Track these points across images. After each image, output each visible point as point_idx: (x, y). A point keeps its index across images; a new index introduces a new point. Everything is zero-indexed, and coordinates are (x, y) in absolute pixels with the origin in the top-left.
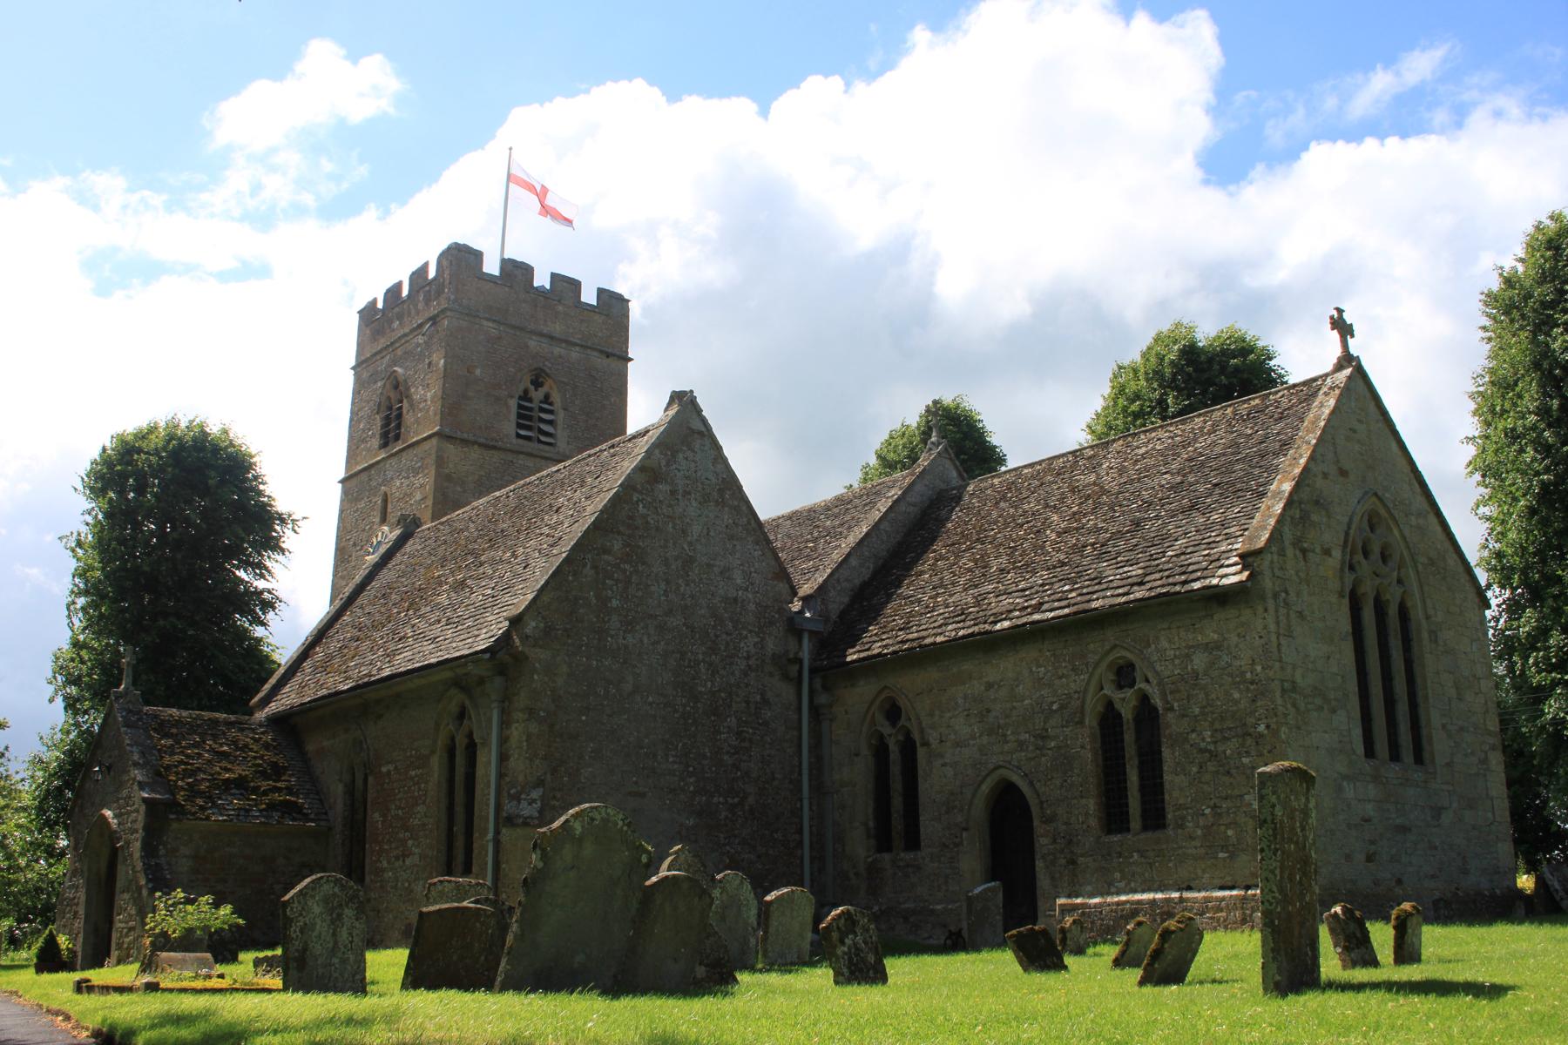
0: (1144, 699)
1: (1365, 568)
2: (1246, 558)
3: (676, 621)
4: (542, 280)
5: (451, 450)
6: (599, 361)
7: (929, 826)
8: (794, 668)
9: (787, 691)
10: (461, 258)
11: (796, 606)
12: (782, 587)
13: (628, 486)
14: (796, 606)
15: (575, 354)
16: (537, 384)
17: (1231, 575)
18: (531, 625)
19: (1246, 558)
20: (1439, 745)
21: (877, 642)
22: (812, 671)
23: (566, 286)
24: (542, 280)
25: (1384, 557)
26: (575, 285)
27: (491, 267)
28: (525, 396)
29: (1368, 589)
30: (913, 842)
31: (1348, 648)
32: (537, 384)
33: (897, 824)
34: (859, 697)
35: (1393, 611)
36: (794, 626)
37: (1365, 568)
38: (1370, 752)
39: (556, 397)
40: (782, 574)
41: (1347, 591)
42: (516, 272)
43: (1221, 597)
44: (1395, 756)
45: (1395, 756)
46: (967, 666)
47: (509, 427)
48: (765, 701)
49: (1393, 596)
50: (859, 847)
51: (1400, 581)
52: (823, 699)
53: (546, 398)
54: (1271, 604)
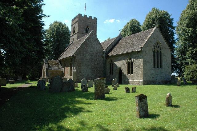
0: (132, 61)
1: (156, 48)
2: (141, 48)
3: (91, 53)
4: (88, 17)
5: (79, 34)
6: (94, 24)
7: (114, 73)
8: (103, 57)
9: (102, 59)
10: (80, 15)
11: (104, 51)
12: (102, 49)
13: (86, 40)
14: (104, 51)
15: (91, 24)
16: (87, 27)
17: (140, 50)
18: (76, 54)
19: (141, 48)
20: (163, 66)
21: (110, 54)
22: (105, 57)
23: (90, 17)
24: (88, 17)
25: (159, 47)
26: (91, 17)
27: (83, 16)
28: (86, 28)
29: (156, 51)
30: (113, 74)
31: (153, 57)
32: (87, 27)
33: (112, 72)
34: (109, 60)
35: (159, 53)
36: (103, 52)
37: (156, 48)
38: (154, 67)
39: (89, 28)
40: (102, 48)
41: (153, 51)
42: (85, 16)
43: (139, 52)
44: (158, 67)
45: (158, 67)
46: (118, 57)
47: (85, 31)
48: (100, 60)
49: (159, 51)
50: (109, 74)
51: (160, 49)
52: (106, 60)
53: (88, 28)
54: (143, 53)
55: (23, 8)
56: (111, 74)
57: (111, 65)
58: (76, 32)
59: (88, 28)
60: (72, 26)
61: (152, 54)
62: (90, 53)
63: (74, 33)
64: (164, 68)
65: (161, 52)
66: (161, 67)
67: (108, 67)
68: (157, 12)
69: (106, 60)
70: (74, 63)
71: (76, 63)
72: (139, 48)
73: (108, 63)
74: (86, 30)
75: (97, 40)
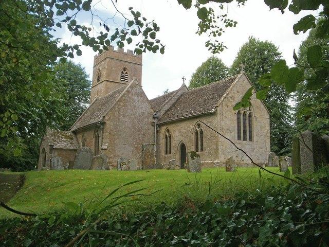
7: (172, 151)
9: (153, 128)
20: (255, 138)
28: (122, 73)
30: (170, 153)
31: (236, 123)
33: (168, 150)
38: (239, 138)
39: (128, 73)
45: (245, 139)
50: (163, 153)
53: (126, 73)
55: (47, 118)
56: (167, 154)
57: (197, 133)
58: (102, 80)
59: (126, 73)
60: (94, 67)
61: (235, 117)
62: (132, 116)
63: (99, 80)
64: (257, 141)
65: (250, 115)
66: (251, 139)
67: (162, 141)
68: (252, 41)
69: (158, 129)
70: (103, 133)
71: (107, 134)
72: (212, 108)
73: (162, 136)
74: (122, 77)
75: (142, 94)
